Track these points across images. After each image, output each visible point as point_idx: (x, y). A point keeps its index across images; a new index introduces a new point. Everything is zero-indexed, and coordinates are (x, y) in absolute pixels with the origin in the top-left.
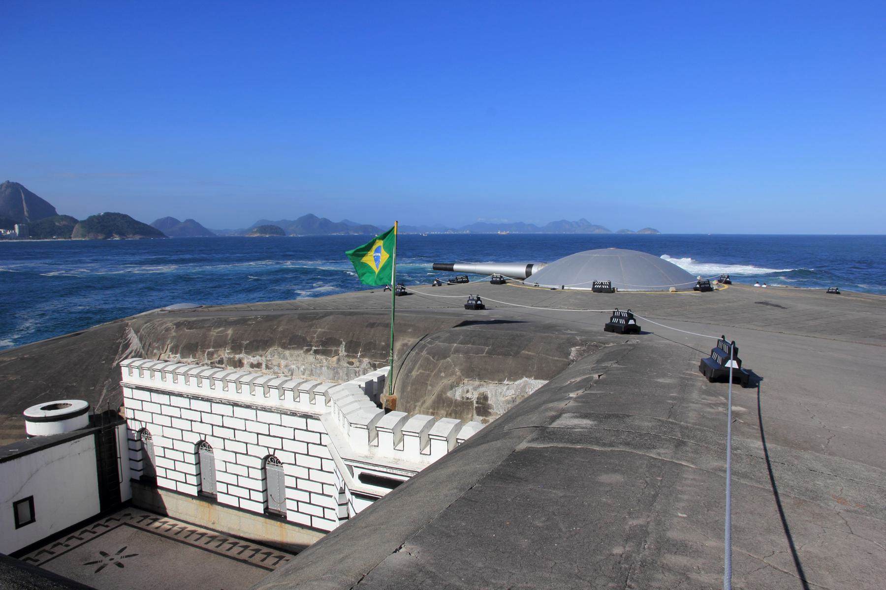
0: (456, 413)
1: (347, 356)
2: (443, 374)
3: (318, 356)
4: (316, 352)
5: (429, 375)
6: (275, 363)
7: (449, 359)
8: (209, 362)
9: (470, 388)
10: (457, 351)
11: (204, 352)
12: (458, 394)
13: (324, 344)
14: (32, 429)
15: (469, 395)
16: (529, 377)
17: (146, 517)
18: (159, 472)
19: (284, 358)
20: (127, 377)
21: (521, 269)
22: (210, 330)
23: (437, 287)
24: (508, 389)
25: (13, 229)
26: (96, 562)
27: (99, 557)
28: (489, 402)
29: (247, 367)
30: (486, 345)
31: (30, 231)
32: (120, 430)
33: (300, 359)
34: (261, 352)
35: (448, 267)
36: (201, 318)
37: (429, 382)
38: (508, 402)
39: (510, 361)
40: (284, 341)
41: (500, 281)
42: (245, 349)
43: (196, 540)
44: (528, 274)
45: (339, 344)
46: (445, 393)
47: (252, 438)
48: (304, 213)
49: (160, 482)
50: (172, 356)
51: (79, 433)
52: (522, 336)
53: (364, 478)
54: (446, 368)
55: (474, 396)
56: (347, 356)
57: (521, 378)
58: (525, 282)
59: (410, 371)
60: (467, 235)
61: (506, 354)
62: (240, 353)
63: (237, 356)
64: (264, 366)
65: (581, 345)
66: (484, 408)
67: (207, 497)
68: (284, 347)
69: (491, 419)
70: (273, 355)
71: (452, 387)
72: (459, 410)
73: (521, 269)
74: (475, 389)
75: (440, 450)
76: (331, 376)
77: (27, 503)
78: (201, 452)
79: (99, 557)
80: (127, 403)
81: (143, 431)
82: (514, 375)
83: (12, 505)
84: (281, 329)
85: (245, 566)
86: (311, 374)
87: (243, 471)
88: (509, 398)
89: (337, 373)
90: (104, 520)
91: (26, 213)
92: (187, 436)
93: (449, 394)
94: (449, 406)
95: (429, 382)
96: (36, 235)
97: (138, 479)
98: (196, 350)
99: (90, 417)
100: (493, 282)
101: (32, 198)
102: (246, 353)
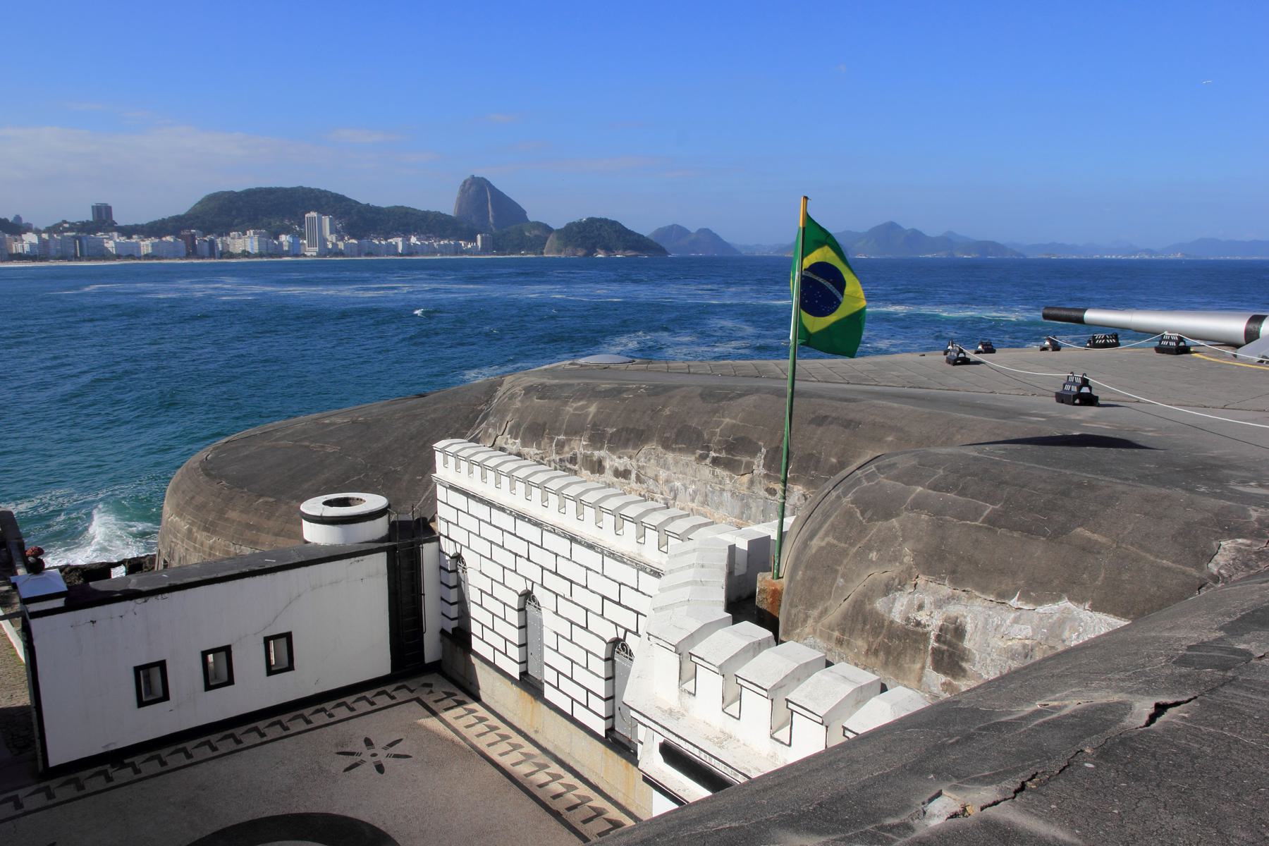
0: (888, 652)
1: (767, 476)
2: (873, 556)
3: (718, 471)
4: (716, 462)
5: (844, 553)
6: (651, 473)
7: (894, 522)
8: (557, 458)
9: (928, 600)
10: (918, 505)
11: (552, 439)
12: (898, 608)
13: (731, 447)
14: (314, 534)
15: (922, 617)
16: (1078, 599)
17: (449, 695)
18: (475, 628)
19: (665, 466)
20: (444, 470)
21: (1235, 325)
22: (566, 403)
23: (1050, 353)
24: (1016, 621)
25: (475, 241)
26: (352, 754)
27: (359, 746)
28: (967, 644)
29: (608, 476)
30: (989, 498)
31: (495, 244)
32: (428, 550)
33: (689, 471)
34: (630, 451)
35: (1074, 314)
36: (563, 382)
37: (840, 569)
38: (1013, 655)
39: (1038, 550)
40: (667, 435)
41: (1179, 347)
42: (609, 442)
43: (501, 755)
44: (1251, 336)
45: (754, 451)
46: (872, 602)
47: (594, 603)
48: (879, 219)
49: (476, 645)
50: (510, 441)
51: (365, 547)
52: (1092, 487)
53: (671, 754)
54: (885, 542)
55: (933, 621)
56: (767, 476)
57: (1056, 599)
58: (1240, 353)
59: (811, 537)
60: (1177, 262)
61: (1030, 531)
62: (601, 448)
63: (597, 454)
64: (633, 476)
65: (1257, 535)
66: (951, 655)
67: (532, 686)
68: (667, 445)
69: (964, 685)
70: (648, 458)
71: (888, 589)
72: (892, 646)
73: (1235, 325)
74: (939, 604)
75: (809, 741)
76: (737, 511)
77: (283, 641)
78: (529, 608)
79: (359, 746)
80: (442, 511)
81: (458, 558)
82: (1040, 588)
83: (262, 641)
84: (667, 412)
85: (554, 823)
86: (705, 503)
87: (580, 656)
88: (1015, 644)
89: (748, 506)
90: (394, 686)
91: (491, 219)
92: (511, 579)
93: (879, 604)
94: (875, 632)
95: (840, 569)
96: (501, 250)
98: (542, 436)
99: (392, 525)
100: (1160, 350)
101: (499, 198)
102: (610, 449)
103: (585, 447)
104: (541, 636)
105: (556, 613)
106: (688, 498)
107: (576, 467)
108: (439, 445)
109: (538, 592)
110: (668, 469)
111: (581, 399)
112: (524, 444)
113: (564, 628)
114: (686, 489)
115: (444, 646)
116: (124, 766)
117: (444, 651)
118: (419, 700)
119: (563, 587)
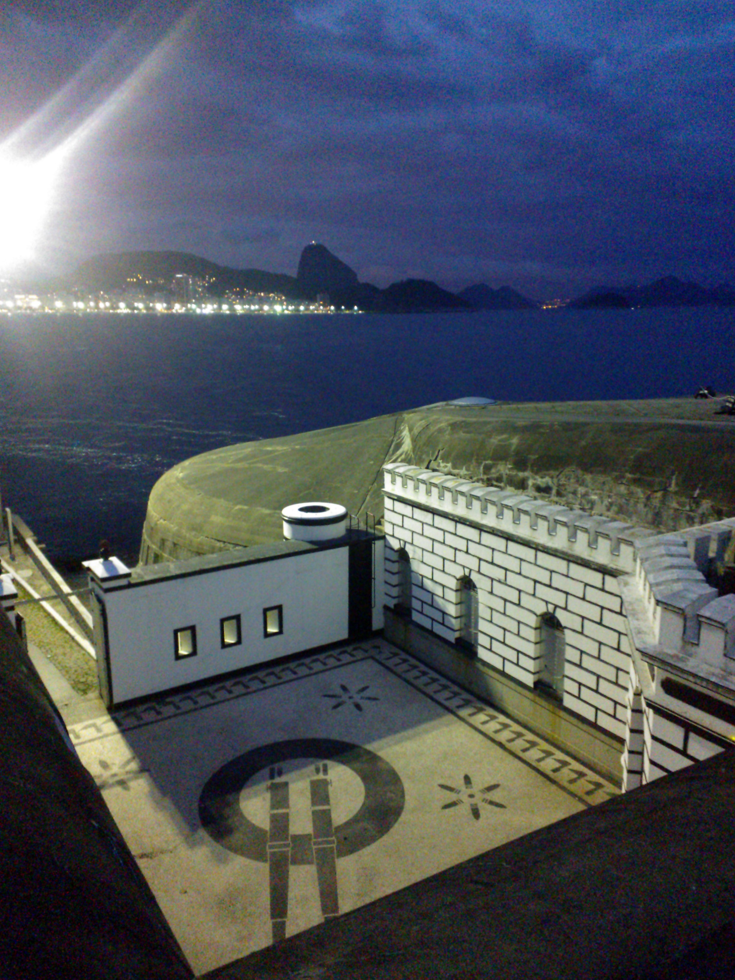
8: (485, 477)
19: (582, 483)
20: (390, 486)
22: (490, 437)
32: (378, 546)
47: (528, 586)
50: (442, 465)
62: (524, 470)
63: (521, 474)
64: (554, 492)
80: (388, 515)
83: (261, 611)
92: (450, 567)
97: (392, 607)
103: (511, 469)
104: (477, 609)
105: (491, 593)
106: (604, 508)
107: (502, 485)
108: (389, 466)
109: (475, 577)
110: (587, 486)
111: (502, 434)
112: (454, 467)
113: (498, 604)
114: (602, 502)
115: (385, 617)
116: (167, 704)
117: (386, 622)
118: (373, 658)
119: (499, 574)
